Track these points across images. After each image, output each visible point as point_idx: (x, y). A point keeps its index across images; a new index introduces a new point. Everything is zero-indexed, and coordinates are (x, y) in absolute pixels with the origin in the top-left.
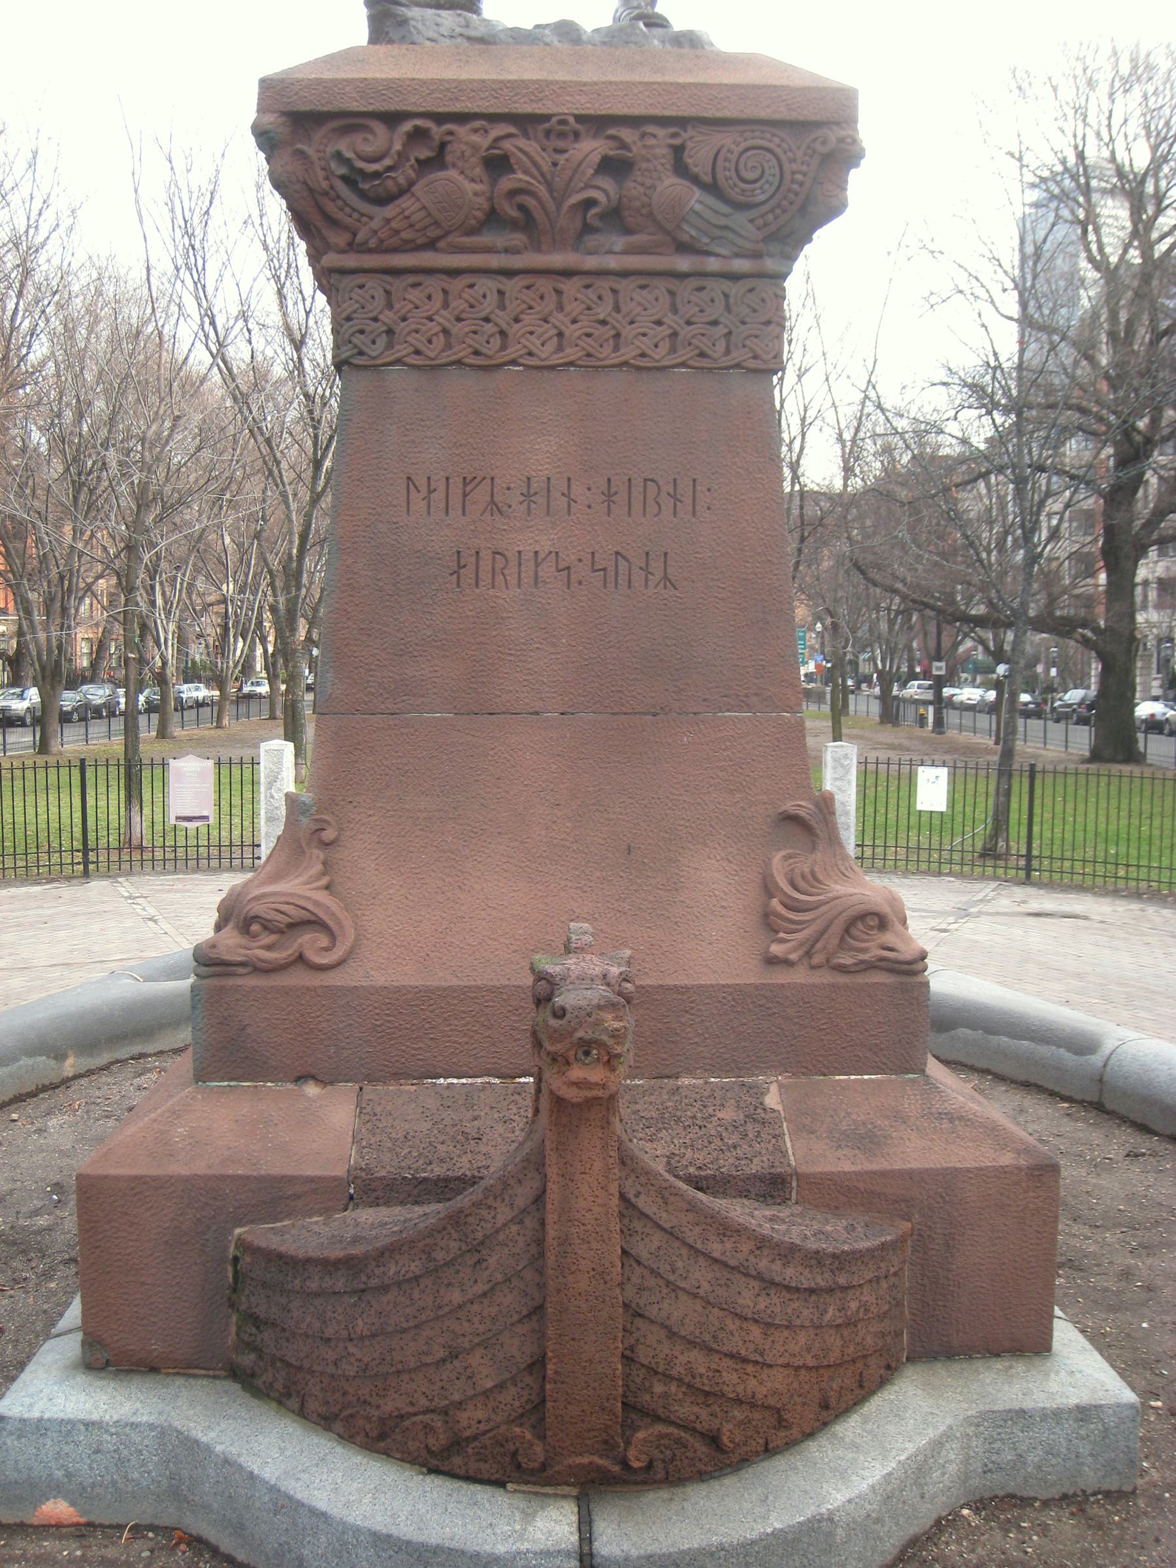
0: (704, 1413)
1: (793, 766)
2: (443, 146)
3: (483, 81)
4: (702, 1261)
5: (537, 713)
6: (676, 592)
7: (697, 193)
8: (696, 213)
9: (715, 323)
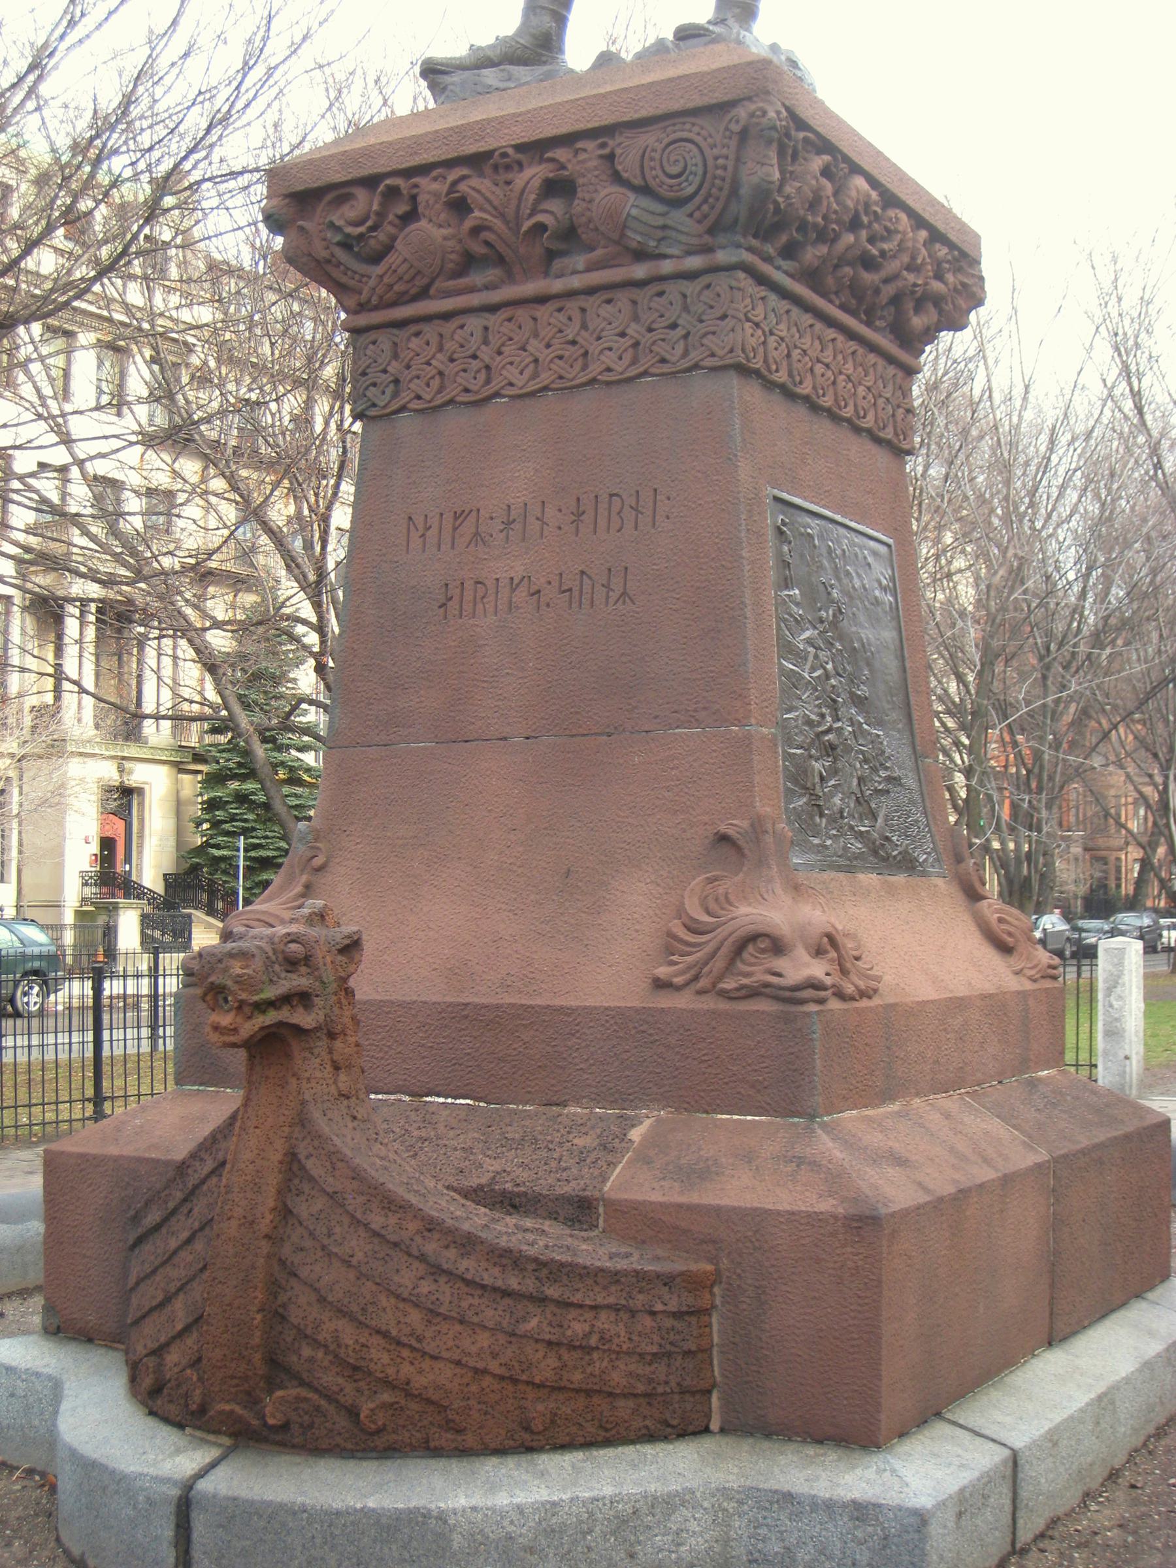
0: (349, 1388)
1: (738, 783)
2: (414, 198)
3: (436, 132)
4: (362, 1232)
5: (505, 739)
6: (633, 607)
7: (632, 196)
8: (635, 218)
9: (674, 326)
